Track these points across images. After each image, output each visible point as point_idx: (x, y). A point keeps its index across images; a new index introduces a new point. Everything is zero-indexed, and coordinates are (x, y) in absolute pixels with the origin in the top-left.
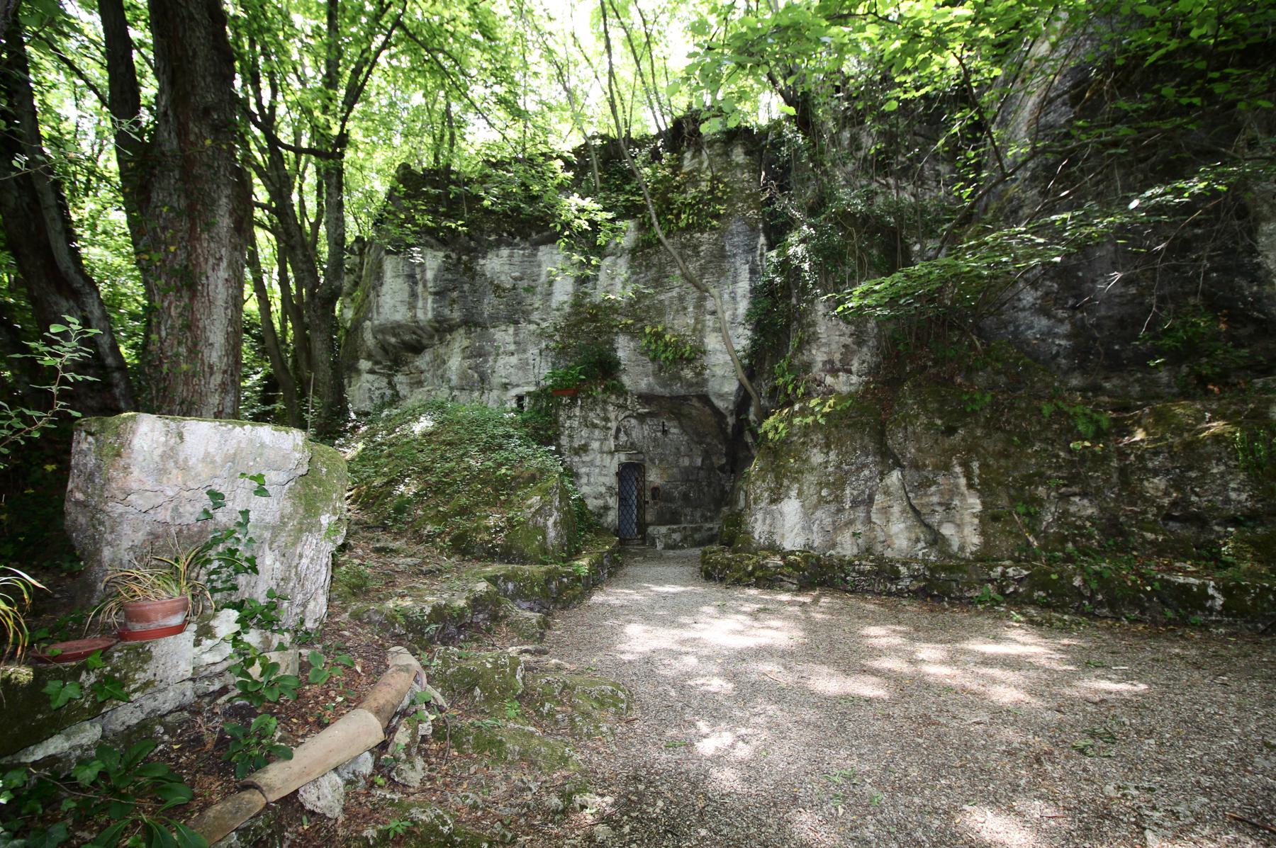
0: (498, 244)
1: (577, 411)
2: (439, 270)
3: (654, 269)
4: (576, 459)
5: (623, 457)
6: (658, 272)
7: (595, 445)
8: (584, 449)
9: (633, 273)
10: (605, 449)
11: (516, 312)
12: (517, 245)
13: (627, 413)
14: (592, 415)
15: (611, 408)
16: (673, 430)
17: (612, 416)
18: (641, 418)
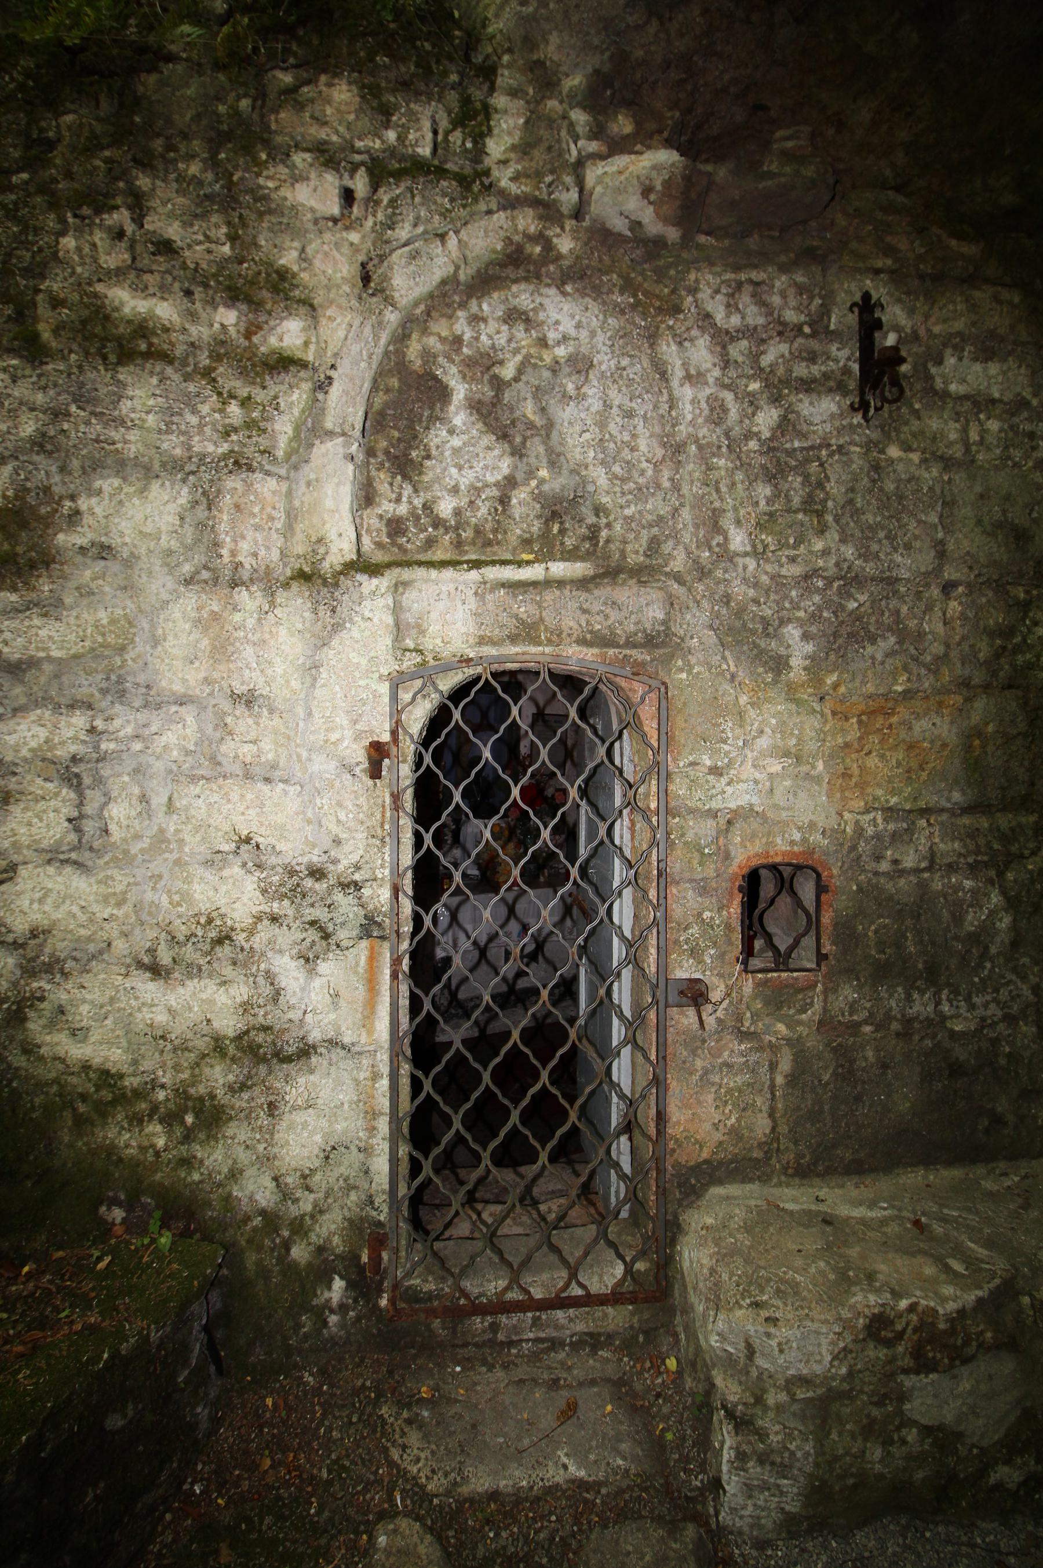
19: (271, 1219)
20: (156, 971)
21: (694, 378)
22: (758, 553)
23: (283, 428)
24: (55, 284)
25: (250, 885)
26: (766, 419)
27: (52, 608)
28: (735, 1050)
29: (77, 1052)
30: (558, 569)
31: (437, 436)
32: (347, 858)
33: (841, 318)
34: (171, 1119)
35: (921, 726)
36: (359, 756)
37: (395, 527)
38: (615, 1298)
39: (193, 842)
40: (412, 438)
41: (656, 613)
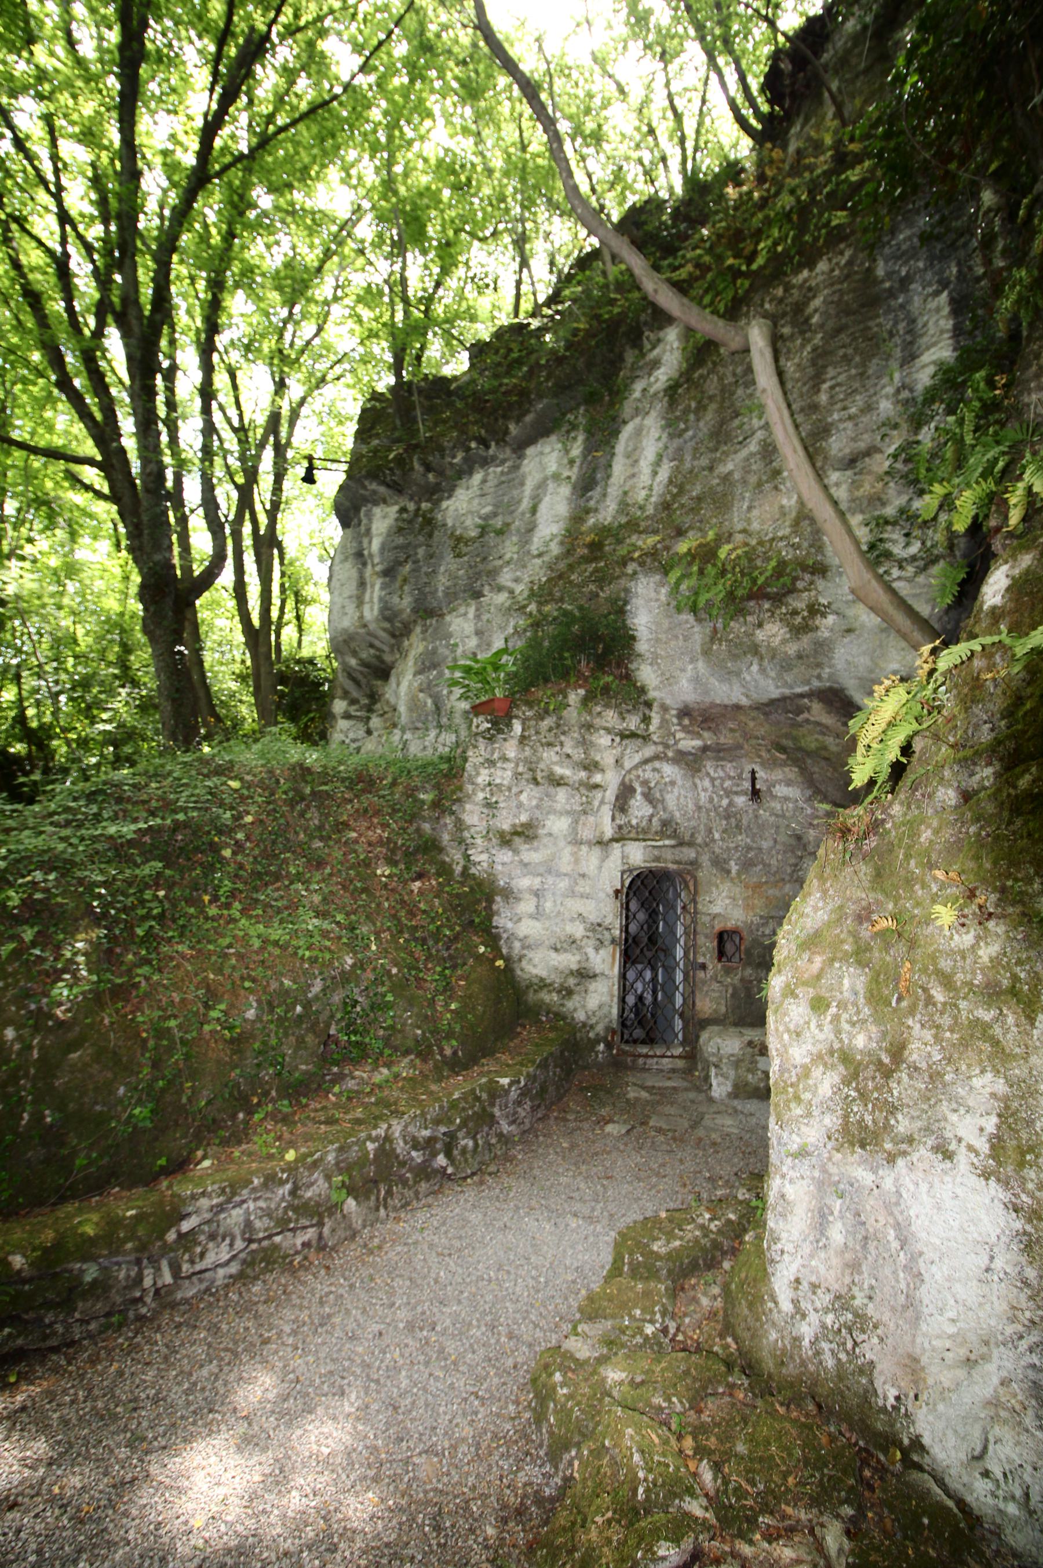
0: (465, 471)
1: (511, 750)
2: (388, 535)
3: (713, 406)
4: (504, 856)
5: (637, 855)
6: (721, 409)
7: (558, 825)
8: (526, 833)
9: (671, 436)
10: (586, 833)
11: (478, 575)
12: (494, 458)
13: (649, 751)
14: (549, 756)
15: (603, 740)
16: (781, 790)
17: (607, 758)
18: (691, 762)
19: (584, 1025)
20: (556, 950)
21: (705, 790)
22: (722, 839)
23: (596, 803)
24: (542, 766)
25: (581, 927)
26: (725, 802)
27: (536, 850)
28: (715, 986)
29: (535, 971)
30: (667, 842)
31: (632, 802)
32: (608, 921)
33: (747, 775)
34: (559, 992)
35: (771, 892)
36: (611, 892)
37: (620, 827)
38: (679, 1057)
39: (567, 915)
40: (625, 803)
41: (693, 855)
